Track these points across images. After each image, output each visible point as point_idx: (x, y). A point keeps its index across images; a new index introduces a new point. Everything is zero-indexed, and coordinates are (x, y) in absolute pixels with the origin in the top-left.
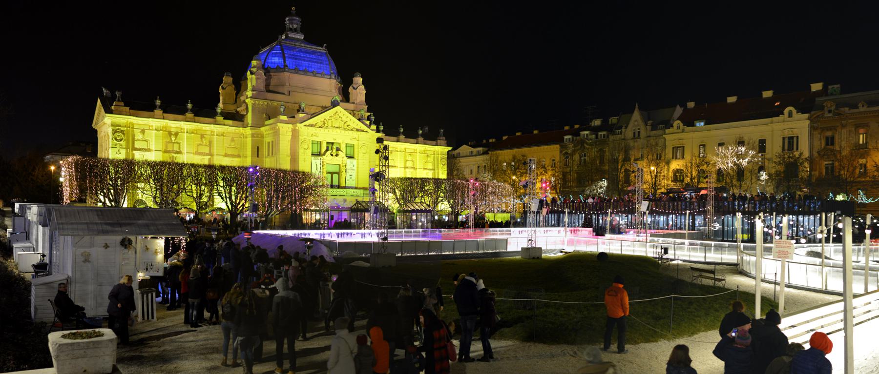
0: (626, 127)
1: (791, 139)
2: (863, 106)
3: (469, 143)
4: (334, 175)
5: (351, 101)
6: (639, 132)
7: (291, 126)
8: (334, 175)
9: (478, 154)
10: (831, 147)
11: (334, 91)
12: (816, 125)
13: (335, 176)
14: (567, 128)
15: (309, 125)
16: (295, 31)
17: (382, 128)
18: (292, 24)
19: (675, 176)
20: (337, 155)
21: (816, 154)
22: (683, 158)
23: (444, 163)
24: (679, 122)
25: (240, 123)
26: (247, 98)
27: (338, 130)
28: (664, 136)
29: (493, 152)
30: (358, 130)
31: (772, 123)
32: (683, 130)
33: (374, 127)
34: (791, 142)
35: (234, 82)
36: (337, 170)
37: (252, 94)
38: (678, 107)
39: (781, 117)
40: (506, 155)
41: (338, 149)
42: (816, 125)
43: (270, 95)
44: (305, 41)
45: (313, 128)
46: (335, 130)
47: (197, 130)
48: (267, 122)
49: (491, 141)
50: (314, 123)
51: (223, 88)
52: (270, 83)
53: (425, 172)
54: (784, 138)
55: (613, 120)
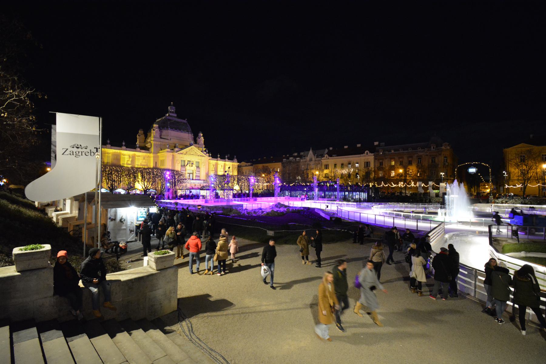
0: (307, 156)
1: (367, 163)
2: (401, 150)
3: (245, 161)
5: (197, 143)
6: (312, 159)
7: (172, 153)
9: (249, 166)
10: (382, 166)
11: (190, 139)
12: (376, 158)
13: (191, 175)
14: (284, 156)
15: (180, 154)
16: (173, 112)
17: (211, 155)
18: (172, 109)
19: (326, 176)
20: (192, 166)
21: (376, 169)
22: (328, 169)
24: (327, 155)
25: (148, 151)
26: (151, 140)
27: (192, 155)
28: (321, 160)
29: (255, 165)
30: (201, 156)
31: (360, 156)
32: (328, 158)
33: (208, 155)
34: (367, 164)
35: (144, 133)
36: (192, 172)
37: (154, 139)
38: (326, 149)
39: (364, 155)
40: (260, 166)
42: (376, 158)
43: (162, 140)
45: (182, 155)
46: (191, 156)
48: (160, 151)
49: (254, 160)
50: (182, 153)
51: (139, 136)
52: (162, 134)
54: (365, 162)
55: (302, 153)
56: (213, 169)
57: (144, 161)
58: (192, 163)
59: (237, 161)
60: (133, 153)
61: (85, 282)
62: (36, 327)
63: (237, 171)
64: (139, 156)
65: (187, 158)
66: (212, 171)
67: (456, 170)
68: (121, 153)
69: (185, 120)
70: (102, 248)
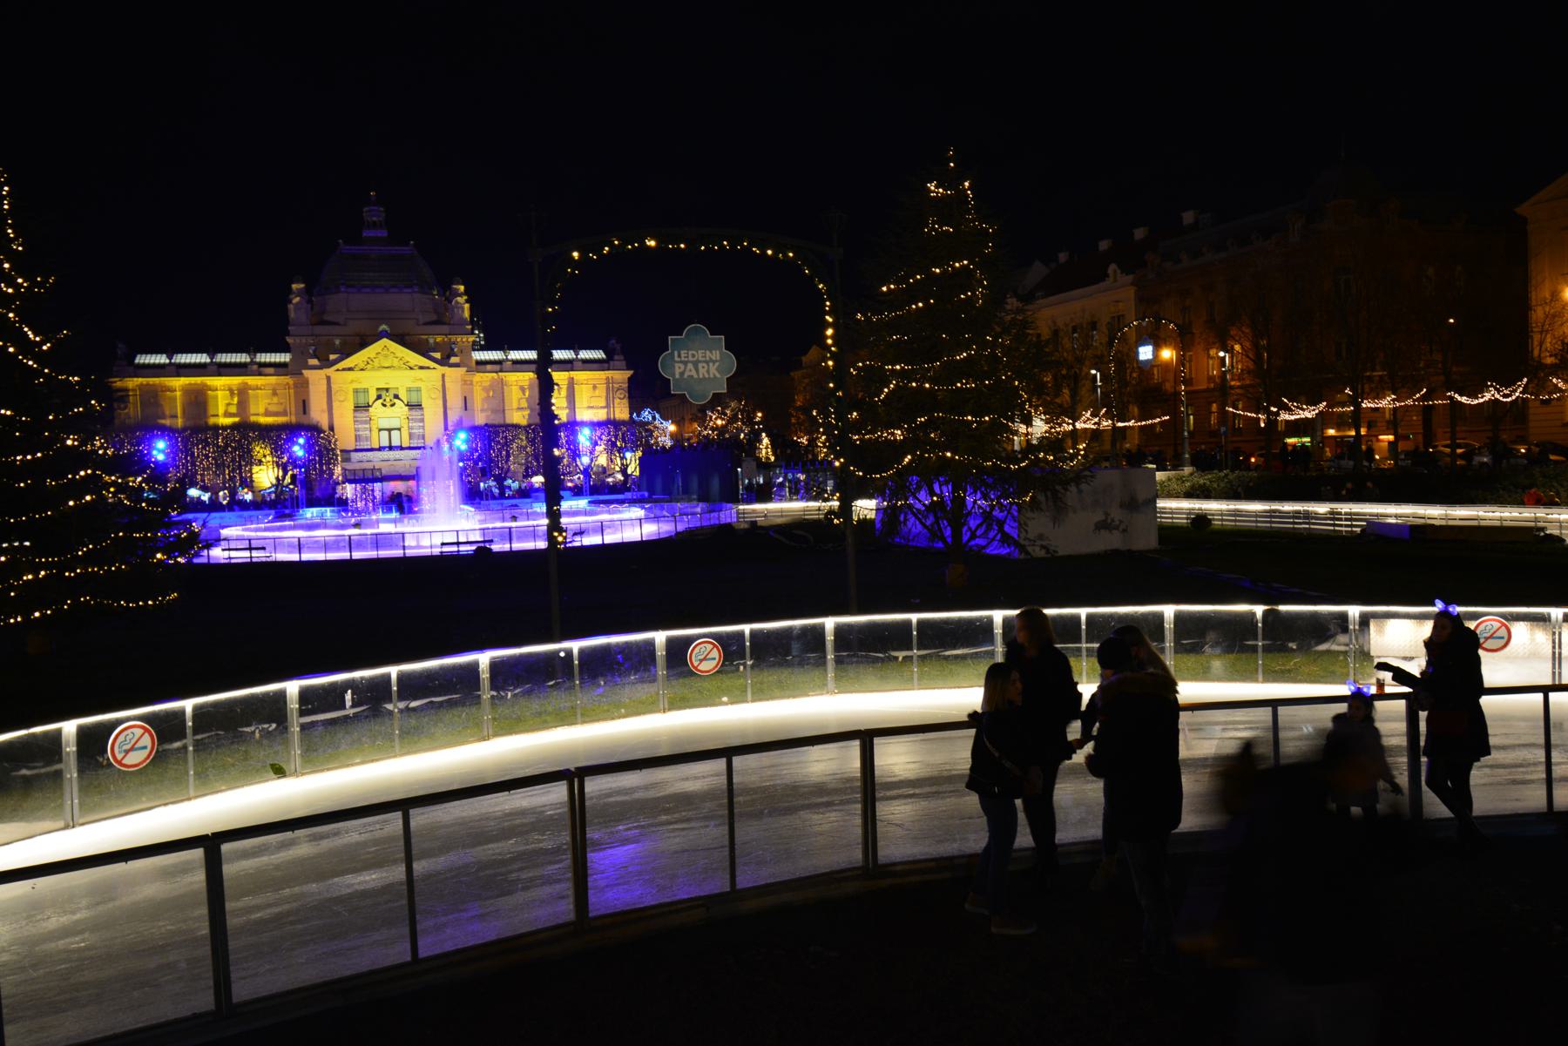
4: (392, 432)
8: (392, 432)
15: (344, 370)
20: (393, 405)
23: (622, 396)
41: (396, 397)
43: (319, 329)
53: (590, 411)
56: (524, 404)
57: (275, 400)
59: (624, 363)
60: (240, 381)
62: (565, 782)
63: (626, 401)
64: (257, 388)
65: (371, 381)
66: (520, 409)
67: (88, 498)
68: (205, 385)
69: (407, 244)
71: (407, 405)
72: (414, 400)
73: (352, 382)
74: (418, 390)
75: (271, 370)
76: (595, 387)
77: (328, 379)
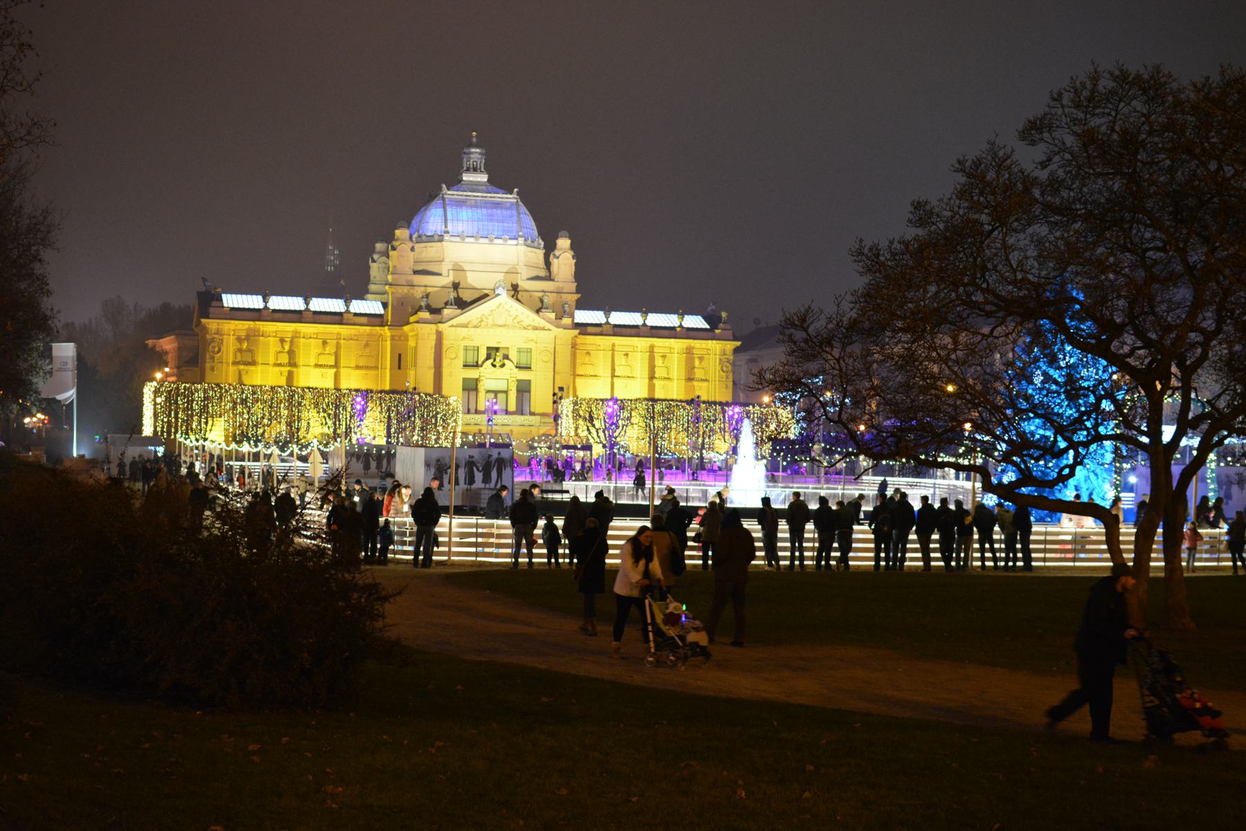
8: (499, 395)
20: (503, 366)
30: (536, 328)
41: (506, 357)
44: (490, 188)
47: (276, 332)
58: (506, 352)
61: (189, 517)
70: (1187, 551)
71: (517, 367)
72: (523, 362)
73: (464, 338)
74: (529, 351)
75: (364, 320)
76: (325, 343)
77: (439, 336)
